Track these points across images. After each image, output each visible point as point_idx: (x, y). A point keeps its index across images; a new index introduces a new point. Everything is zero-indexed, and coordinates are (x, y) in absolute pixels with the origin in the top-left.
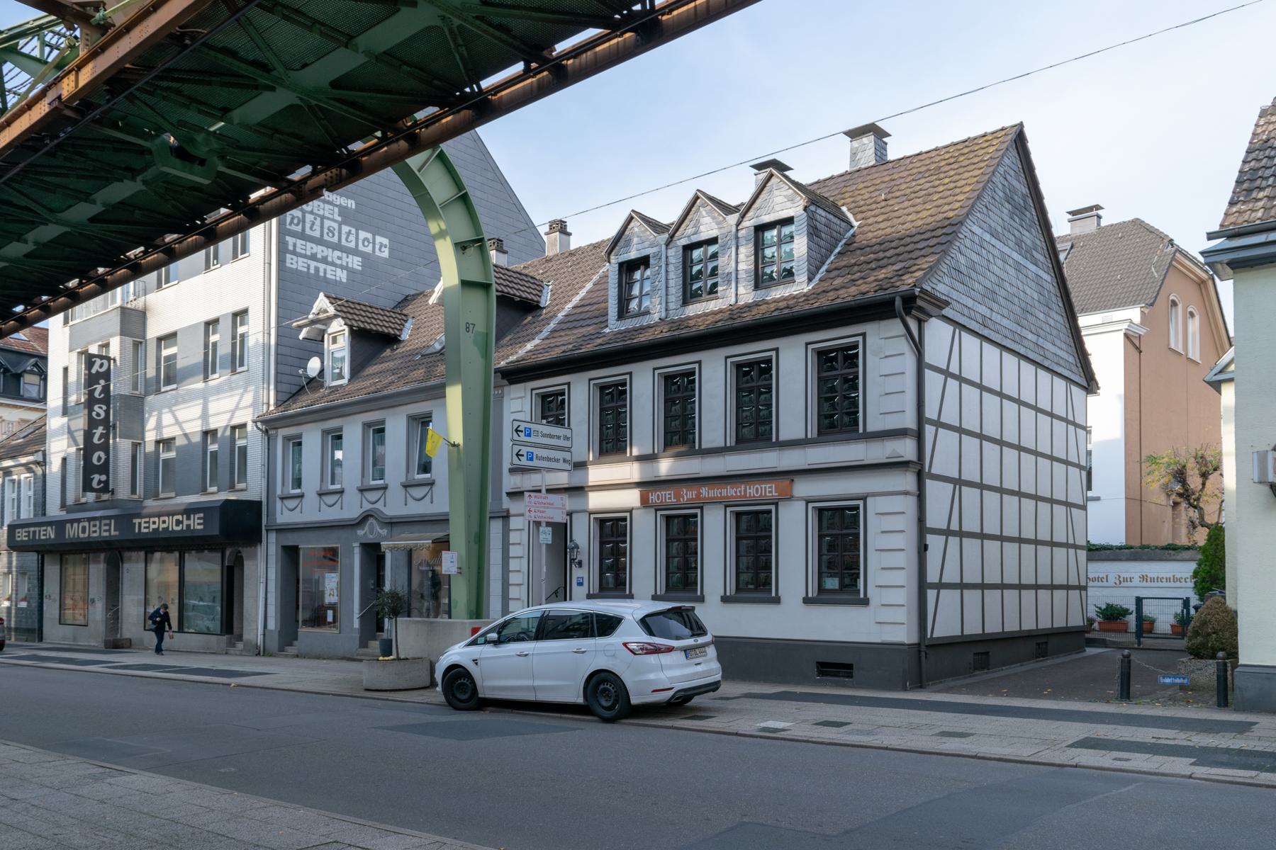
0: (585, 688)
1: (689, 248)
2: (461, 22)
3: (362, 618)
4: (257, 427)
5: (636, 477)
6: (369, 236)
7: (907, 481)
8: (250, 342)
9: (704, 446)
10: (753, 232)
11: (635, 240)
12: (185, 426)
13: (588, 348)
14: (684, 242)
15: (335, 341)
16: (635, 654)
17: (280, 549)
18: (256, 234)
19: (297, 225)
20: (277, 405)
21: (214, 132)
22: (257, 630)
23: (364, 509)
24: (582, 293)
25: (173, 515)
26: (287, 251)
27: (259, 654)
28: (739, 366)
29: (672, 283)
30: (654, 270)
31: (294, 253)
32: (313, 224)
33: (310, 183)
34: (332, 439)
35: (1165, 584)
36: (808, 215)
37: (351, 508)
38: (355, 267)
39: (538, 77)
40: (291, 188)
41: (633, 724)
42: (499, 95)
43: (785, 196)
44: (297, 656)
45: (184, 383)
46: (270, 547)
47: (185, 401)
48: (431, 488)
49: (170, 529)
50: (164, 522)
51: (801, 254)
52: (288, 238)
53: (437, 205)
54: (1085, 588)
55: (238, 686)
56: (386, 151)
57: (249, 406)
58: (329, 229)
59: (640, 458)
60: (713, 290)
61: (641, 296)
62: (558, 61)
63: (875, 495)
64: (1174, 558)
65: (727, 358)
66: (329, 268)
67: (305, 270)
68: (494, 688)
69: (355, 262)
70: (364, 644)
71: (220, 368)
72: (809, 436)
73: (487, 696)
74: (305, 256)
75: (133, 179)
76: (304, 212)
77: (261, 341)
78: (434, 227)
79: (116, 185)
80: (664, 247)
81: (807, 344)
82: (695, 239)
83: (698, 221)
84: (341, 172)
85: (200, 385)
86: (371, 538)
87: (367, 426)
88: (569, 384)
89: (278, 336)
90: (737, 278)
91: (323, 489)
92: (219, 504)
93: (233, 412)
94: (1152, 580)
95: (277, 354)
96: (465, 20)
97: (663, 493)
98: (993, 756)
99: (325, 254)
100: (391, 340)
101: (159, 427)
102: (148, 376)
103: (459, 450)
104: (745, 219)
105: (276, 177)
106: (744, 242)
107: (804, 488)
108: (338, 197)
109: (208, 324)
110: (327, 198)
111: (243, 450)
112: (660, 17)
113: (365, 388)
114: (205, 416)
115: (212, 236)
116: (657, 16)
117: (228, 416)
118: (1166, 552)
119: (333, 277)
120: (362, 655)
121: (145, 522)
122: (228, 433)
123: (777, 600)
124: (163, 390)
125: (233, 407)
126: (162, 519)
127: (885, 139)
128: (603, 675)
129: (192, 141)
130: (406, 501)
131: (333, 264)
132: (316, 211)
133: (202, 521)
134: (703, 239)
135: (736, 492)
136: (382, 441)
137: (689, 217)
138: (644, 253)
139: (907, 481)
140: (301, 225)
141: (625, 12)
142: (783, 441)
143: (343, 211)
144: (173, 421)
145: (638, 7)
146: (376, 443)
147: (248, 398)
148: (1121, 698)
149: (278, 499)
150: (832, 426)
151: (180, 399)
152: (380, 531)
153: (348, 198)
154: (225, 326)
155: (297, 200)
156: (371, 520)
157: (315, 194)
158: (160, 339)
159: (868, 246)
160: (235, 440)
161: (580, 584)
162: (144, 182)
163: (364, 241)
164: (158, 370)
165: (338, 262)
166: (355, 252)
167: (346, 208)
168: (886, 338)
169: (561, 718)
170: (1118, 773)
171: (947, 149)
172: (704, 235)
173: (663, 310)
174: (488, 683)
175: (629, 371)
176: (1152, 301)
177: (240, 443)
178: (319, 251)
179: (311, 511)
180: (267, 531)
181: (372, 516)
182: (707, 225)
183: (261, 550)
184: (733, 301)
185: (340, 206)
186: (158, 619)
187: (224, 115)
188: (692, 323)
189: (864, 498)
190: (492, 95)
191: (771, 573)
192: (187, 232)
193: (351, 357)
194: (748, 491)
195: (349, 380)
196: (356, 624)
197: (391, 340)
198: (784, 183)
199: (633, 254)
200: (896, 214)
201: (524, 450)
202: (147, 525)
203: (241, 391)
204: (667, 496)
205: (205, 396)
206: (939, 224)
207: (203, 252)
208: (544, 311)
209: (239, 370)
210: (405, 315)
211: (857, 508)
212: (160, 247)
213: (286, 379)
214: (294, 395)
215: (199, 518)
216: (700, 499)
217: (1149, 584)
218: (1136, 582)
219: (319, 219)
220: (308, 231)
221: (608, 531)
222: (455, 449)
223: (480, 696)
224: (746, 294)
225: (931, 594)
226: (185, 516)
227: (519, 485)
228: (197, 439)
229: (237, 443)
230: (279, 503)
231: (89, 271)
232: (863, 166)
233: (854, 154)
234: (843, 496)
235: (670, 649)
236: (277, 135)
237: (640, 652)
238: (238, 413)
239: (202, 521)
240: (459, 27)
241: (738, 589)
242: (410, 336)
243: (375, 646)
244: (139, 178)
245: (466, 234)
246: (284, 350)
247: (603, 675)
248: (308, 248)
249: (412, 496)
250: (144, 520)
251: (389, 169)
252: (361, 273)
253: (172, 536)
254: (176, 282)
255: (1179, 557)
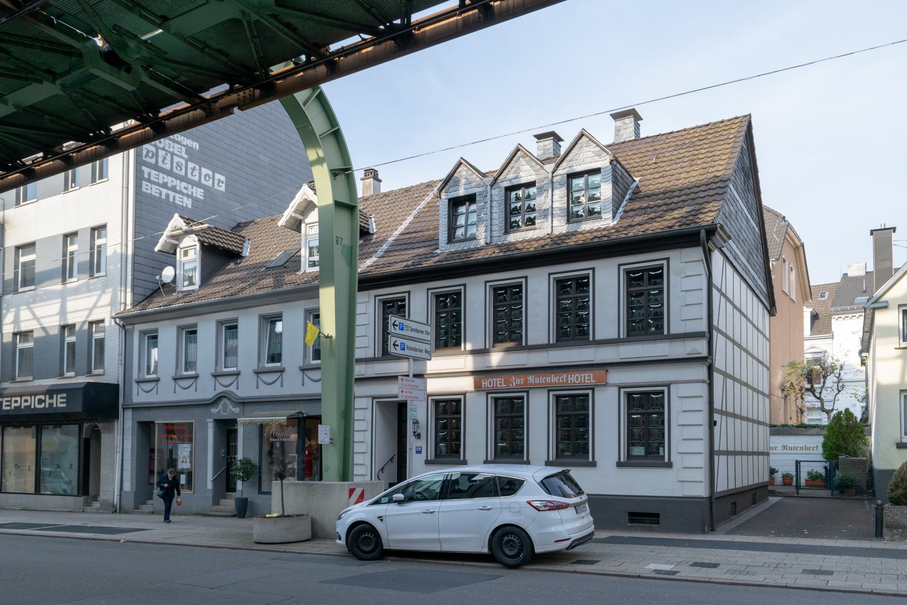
0: (490, 540)
1: (509, 189)
2: (257, 18)
3: (214, 481)
4: (116, 322)
5: (470, 367)
6: (210, 173)
7: (701, 372)
8: (109, 252)
9: (529, 343)
10: (566, 179)
11: (463, 181)
12: (42, 321)
13: (429, 263)
14: (507, 184)
15: (186, 254)
16: (539, 510)
17: (136, 424)
18: (115, 162)
19: (152, 158)
20: (134, 304)
21: (146, 41)
22: (114, 491)
23: (218, 391)
24: (405, 224)
25: (35, 395)
26: (143, 179)
27: (116, 511)
28: (495, 289)
29: (495, 216)
30: (480, 205)
31: (149, 180)
32: (165, 158)
33: (221, 102)
34: (186, 334)
35: (799, 451)
36: (612, 168)
37: (206, 390)
38: (198, 196)
39: (463, 15)
40: (203, 105)
41: (536, 570)
42: (422, 30)
43: (593, 152)
44: (153, 513)
45: (42, 285)
46: (127, 422)
47: (43, 300)
48: (281, 375)
49: (33, 407)
50: (26, 401)
51: (607, 197)
52: (144, 168)
53: (318, 138)
54: (768, 454)
55: (127, 542)
56: (302, 76)
57: (107, 305)
58: (177, 164)
59: (474, 352)
60: (532, 221)
61: (467, 226)
62: (332, 57)
63: (677, 382)
64: (805, 433)
65: (550, 274)
66: (177, 196)
67: (158, 195)
68: (399, 541)
69: (199, 193)
70: (216, 502)
71: (79, 272)
72: (376, 356)
73: (392, 548)
74: (157, 184)
75: (53, 81)
76: (157, 148)
77: (119, 251)
78: (312, 155)
79: (35, 86)
80: (489, 187)
81: (619, 265)
82: (515, 182)
83: (518, 168)
84: (254, 93)
85: (59, 287)
86: (225, 415)
87: (220, 323)
88: (409, 292)
89: (136, 247)
90: (552, 214)
91: (218, 371)
92: (82, 386)
93: (91, 310)
94: (791, 448)
95: (134, 263)
96: (262, 17)
97: (495, 380)
98: (888, 592)
99: (174, 184)
100: (235, 256)
101: (17, 321)
102: (6, 278)
103: (331, 341)
104: (559, 168)
105: (191, 93)
106: (559, 186)
107: (617, 377)
108: (185, 139)
109: (66, 236)
110: (176, 139)
111: (101, 343)
112: (413, 31)
113: (218, 292)
114: (63, 312)
115: (69, 163)
116: (411, 31)
117: (86, 313)
118: (800, 429)
119: (181, 204)
120: (215, 511)
121: (7, 401)
122: (86, 327)
123: (593, 464)
124: (20, 290)
125: (91, 306)
126: (24, 398)
127: (639, 122)
128: (508, 528)
129: (124, 46)
130: (257, 385)
131: (180, 192)
132: (167, 148)
133: (65, 400)
134: (522, 182)
135: (559, 380)
136: (235, 336)
137: (511, 165)
138: (471, 192)
139: (701, 372)
140: (154, 158)
141: (388, 24)
142: (598, 341)
143: (189, 150)
144: (31, 317)
145: (398, 21)
146: (228, 337)
147: (106, 298)
148: (876, 536)
149: (134, 383)
150: (566, 334)
151: (38, 299)
152: (233, 409)
153: (193, 140)
154: (85, 238)
155: (207, 116)
156: (225, 400)
157: (226, 111)
158: (18, 248)
159: (654, 195)
160: (16, 344)
161: (419, 452)
162: (63, 86)
163: (205, 176)
164: (16, 274)
165: (185, 191)
166: (198, 184)
167: (192, 148)
168: (686, 262)
169: (463, 565)
170: (68, 524)
171: (695, 130)
172: (524, 180)
173: (489, 237)
174: (393, 537)
175: (668, 256)
176: (778, 257)
177: (96, 336)
178: (170, 181)
179: (167, 393)
180: (124, 409)
181: (225, 397)
182: (526, 173)
183: (118, 426)
184: (549, 231)
185: (186, 146)
186: (166, 485)
187: (162, 22)
188: (519, 246)
189: (668, 385)
190: (415, 29)
191: (523, 443)
192: (89, 141)
193: (202, 268)
194: (569, 379)
195: (200, 287)
196: (210, 486)
197: (235, 256)
198: (470, 170)
199: (462, 192)
200: (669, 173)
201: (399, 342)
202: (9, 403)
203: (99, 292)
204: (498, 382)
205: (63, 297)
206: (711, 181)
207: (63, 174)
208: (375, 236)
209: (96, 275)
210: (243, 237)
211: (522, 398)
212: (58, 154)
213: (141, 283)
214: (148, 297)
215: (61, 398)
216: (528, 385)
217: (788, 451)
218: (779, 450)
219: (169, 155)
220: (160, 164)
221: (441, 410)
222: (328, 340)
223: (384, 548)
224: (560, 227)
225: (716, 457)
226: (47, 396)
227: (363, 372)
228: (55, 332)
229: (94, 336)
230: (135, 386)
231: (54, 147)
232: (626, 140)
233: (618, 130)
234: (644, 384)
235: (566, 506)
236: (207, 49)
237: (544, 508)
238: (95, 311)
239: (65, 400)
240: (257, 21)
241: (436, 456)
242: (250, 253)
243: (229, 504)
244: (58, 82)
245: (338, 165)
246: (140, 260)
247: (508, 528)
248: (161, 178)
249: (142, 389)
250: (5, 399)
251: (277, 101)
252: (203, 202)
253: (35, 412)
254: (35, 200)
255: (809, 433)
